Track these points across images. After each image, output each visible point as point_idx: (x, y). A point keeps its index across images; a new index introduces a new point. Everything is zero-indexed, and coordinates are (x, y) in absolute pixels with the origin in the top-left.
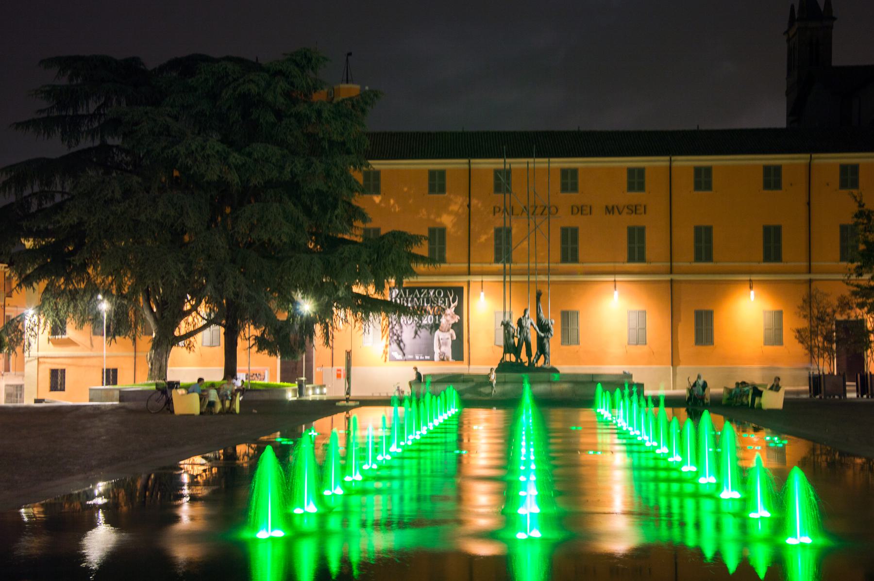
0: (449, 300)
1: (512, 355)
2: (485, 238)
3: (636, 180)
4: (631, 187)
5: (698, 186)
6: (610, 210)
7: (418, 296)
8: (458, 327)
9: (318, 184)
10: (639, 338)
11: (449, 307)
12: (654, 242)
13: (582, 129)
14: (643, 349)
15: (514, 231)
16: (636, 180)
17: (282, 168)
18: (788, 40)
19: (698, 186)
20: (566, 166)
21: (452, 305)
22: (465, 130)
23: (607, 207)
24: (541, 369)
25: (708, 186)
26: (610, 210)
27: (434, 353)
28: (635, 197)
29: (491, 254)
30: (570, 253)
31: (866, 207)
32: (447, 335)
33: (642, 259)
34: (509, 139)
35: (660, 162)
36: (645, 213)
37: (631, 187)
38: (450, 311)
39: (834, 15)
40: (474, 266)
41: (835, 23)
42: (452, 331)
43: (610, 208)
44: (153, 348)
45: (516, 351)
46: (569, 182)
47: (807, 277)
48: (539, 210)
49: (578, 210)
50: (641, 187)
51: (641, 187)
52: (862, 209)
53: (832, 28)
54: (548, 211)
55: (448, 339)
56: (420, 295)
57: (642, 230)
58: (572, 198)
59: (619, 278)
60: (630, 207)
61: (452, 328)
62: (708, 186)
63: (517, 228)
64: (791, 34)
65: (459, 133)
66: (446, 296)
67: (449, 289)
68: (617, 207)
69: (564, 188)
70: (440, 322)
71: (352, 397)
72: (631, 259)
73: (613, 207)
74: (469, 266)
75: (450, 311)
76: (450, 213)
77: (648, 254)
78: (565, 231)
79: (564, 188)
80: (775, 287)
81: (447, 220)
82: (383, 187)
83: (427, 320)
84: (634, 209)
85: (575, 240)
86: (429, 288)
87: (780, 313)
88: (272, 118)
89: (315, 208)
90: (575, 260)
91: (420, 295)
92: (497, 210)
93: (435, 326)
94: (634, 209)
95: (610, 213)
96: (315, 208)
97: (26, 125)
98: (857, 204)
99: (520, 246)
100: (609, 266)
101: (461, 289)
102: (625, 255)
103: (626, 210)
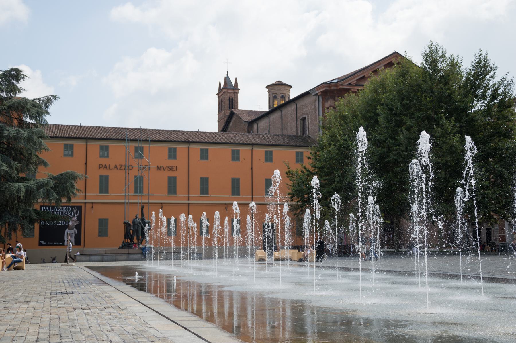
0: (74, 213)
1: (129, 240)
4: (170, 157)
5: (202, 158)
6: (159, 168)
7: (57, 210)
8: (78, 227)
11: (74, 216)
13: (143, 128)
18: (219, 97)
19: (202, 158)
20: (201, 147)
21: (76, 216)
22: (142, 128)
23: (158, 166)
25: (206, 158)
26: (159, 168)
27: (65, 241)
31: (291, 169)
34: (60, 129)
36: (176, 170)
37: (170, 157)
39: (239, 88)
41: (239, 91)
42: (75, 229)
43: (159, 167)
48: (123, 168)
50: (175, 157)
51: (175, 157)
52: (289, 170)
53: (238, 93)
55: (73, 233)
56: (58, 210)
60: (169, 167)
61: (75, 228)
62: (206, 158)
64: (220, 94)
65: (79, 126)
66: (72, 210)
68: (163, 166)
70: (68, 224)
73: (161, 167)
74: (252, 196)
91: (58, 210)
92: (101, 166)
94: (171, 169)
95: (159, 169)
98: (287, 167)
103: (167, 169)
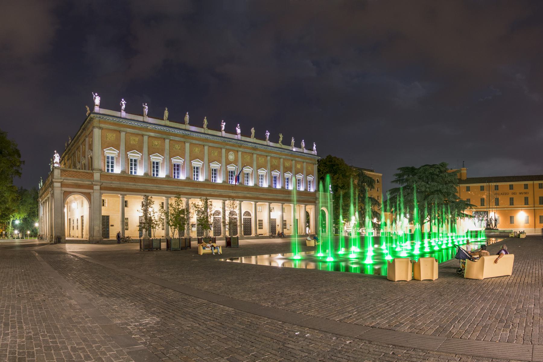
2: (493, 200)
3: (526, 186)
4: (525, 188)
6: (520, 193)
9: (445, 190)
10: (527, 222)
12: (530, 201)
14: (528, 224)
15: (499, 199)
16: (526, 186)
17: (437, 187)
24: (495, 229)
26: (520, 193)
28: (526, 190)
29: (494, 204)
30: (512, 203)
32: (485, 222)
33: (528, 204)
35: (531, 182)
37: (525, 188)
38: (485, 217)
40: (491, 207)
44: (409, 222)
45: (489, 225)
46: (511, 187)
47: (533, 208)
49: (514, 194)
50: (527, 188)
51: (527, 188)
54: (506, 194)
57: (527, 198)
58: (512, 191)
59: (523, 209)
63: (500, 198)
67: (485, 212)
69: (510, 189)
71: (138, 200)
72: (525, 204)
75: (485, 217)
76: (485, 195)
77: (529, 203)
78: (510, 198)
79: (510, 189)
80: (527, 211)
81: (484, 197)
82: (471, 190)
83: (481, 218)
84: (526, 193)
85: (513, 200)
86: (481, 212)
87: (528, 216)
88: (436, 177)
89: (446, 195)
90: (513, 205)
93: (482, 220)
94: (526, 193)
96: (446, 195)
97: (393, 182)
99: (501, 202)
100: (521, 206)
101: (488, 212)
102: (524, 203)
